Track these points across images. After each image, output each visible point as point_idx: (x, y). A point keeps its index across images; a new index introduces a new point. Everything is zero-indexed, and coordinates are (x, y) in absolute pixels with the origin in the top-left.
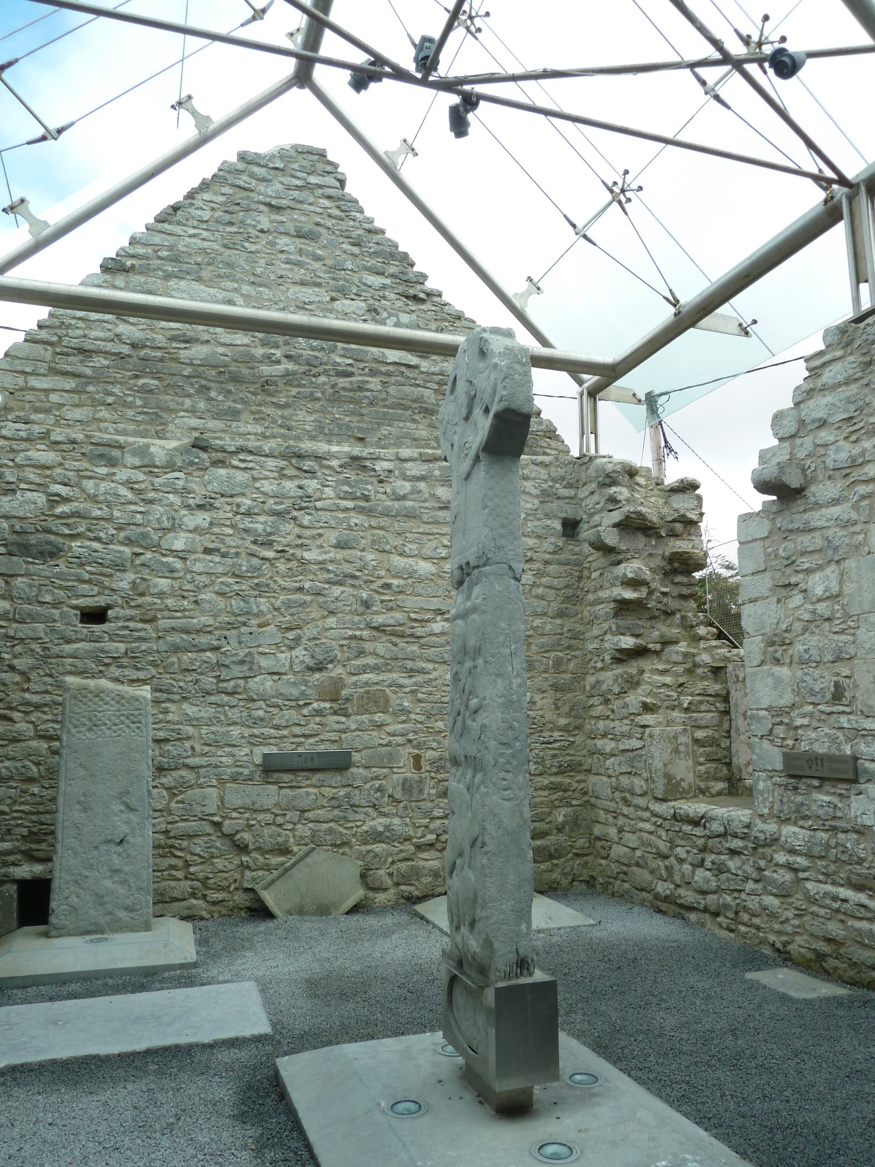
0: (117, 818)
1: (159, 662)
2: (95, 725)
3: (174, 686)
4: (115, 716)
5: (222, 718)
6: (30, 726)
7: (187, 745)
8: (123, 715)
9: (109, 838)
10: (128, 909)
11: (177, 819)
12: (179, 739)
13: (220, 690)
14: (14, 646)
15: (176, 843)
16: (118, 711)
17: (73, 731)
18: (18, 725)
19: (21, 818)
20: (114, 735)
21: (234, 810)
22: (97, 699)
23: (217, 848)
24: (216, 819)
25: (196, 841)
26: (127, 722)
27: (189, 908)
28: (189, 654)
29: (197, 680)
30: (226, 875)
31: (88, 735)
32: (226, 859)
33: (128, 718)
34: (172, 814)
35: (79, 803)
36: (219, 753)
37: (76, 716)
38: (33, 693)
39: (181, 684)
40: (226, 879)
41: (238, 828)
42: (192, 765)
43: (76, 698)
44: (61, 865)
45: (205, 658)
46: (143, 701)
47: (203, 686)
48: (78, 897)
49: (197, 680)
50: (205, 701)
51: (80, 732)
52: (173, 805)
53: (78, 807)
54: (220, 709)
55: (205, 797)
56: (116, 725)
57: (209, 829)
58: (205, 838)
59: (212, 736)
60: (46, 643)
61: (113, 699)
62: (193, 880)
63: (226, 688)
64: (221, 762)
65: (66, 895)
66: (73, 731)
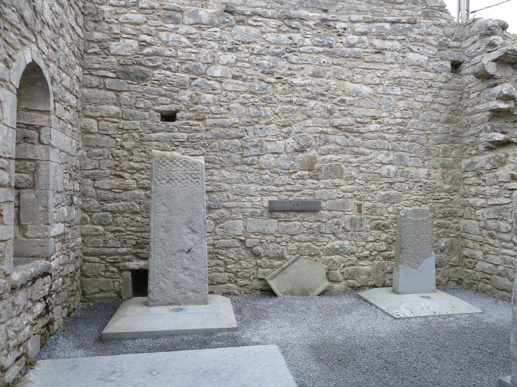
0: (186, 237)
1: (207, 145)
2: (171, 180)
3: (216, 160)
4: (183, 174)
5: (245, 179)
6: (134, 181)
7: (225, 194)
8: (188, 174)
9: (181, 249)
10: (194, 291)
11: (220, 237)
12: (220, 191)
13: (243, 162)
14: (123, 134)
15: (219, 251)
16: (185, 171)
17: (158, 183)
18: (127, 181)
19: (132, 235)
20: (183, 186)
21: (252, 233)
22: (171, 163)
23: (243, 255)
24: (242, 238)
25: (231, 250)
26: (190, 178)
27: (227, 288)
28: (225, 140)
29: (229, 156)
30: (248, 270)
31: (167, 185)
32: (248, 261)
33: (191, 176)
34: (217, 235)
35: (163, 227)
36: (243, 200)
37: (160, 174)
38: (135, 162)
39: (221, 158)
40: (248, 272)
41: (254, 244)
42: (227, 206)
43: (158, 162)
44: (153, 264)
45: (234, 143)
46: (200, 165)
47: (233, 160)
48: (164, 283)
49: (229, 156)
50: (234, 169)
51: (162, 184)
52: (217, 229)
53: (162, 229)
54: (243, 174)
55: (235, 225)
56: (183, 180)
57: (238, 244)
58: (236, 249)
59: (239, 190)
60: (141, 132)
61: (181, 164)
62: (229, 272)
63: (247, 161)
64: (244, 205)
65: (157, 282)
66: (158, 183)
